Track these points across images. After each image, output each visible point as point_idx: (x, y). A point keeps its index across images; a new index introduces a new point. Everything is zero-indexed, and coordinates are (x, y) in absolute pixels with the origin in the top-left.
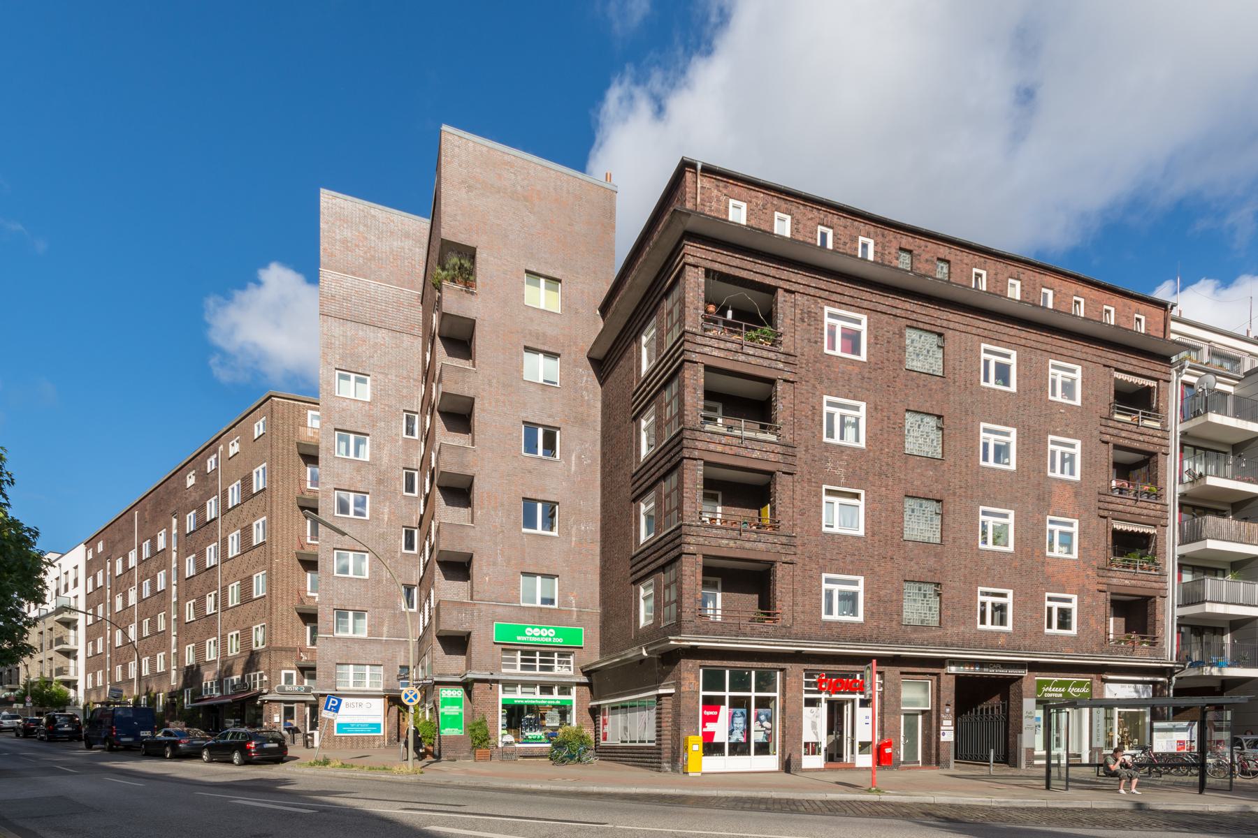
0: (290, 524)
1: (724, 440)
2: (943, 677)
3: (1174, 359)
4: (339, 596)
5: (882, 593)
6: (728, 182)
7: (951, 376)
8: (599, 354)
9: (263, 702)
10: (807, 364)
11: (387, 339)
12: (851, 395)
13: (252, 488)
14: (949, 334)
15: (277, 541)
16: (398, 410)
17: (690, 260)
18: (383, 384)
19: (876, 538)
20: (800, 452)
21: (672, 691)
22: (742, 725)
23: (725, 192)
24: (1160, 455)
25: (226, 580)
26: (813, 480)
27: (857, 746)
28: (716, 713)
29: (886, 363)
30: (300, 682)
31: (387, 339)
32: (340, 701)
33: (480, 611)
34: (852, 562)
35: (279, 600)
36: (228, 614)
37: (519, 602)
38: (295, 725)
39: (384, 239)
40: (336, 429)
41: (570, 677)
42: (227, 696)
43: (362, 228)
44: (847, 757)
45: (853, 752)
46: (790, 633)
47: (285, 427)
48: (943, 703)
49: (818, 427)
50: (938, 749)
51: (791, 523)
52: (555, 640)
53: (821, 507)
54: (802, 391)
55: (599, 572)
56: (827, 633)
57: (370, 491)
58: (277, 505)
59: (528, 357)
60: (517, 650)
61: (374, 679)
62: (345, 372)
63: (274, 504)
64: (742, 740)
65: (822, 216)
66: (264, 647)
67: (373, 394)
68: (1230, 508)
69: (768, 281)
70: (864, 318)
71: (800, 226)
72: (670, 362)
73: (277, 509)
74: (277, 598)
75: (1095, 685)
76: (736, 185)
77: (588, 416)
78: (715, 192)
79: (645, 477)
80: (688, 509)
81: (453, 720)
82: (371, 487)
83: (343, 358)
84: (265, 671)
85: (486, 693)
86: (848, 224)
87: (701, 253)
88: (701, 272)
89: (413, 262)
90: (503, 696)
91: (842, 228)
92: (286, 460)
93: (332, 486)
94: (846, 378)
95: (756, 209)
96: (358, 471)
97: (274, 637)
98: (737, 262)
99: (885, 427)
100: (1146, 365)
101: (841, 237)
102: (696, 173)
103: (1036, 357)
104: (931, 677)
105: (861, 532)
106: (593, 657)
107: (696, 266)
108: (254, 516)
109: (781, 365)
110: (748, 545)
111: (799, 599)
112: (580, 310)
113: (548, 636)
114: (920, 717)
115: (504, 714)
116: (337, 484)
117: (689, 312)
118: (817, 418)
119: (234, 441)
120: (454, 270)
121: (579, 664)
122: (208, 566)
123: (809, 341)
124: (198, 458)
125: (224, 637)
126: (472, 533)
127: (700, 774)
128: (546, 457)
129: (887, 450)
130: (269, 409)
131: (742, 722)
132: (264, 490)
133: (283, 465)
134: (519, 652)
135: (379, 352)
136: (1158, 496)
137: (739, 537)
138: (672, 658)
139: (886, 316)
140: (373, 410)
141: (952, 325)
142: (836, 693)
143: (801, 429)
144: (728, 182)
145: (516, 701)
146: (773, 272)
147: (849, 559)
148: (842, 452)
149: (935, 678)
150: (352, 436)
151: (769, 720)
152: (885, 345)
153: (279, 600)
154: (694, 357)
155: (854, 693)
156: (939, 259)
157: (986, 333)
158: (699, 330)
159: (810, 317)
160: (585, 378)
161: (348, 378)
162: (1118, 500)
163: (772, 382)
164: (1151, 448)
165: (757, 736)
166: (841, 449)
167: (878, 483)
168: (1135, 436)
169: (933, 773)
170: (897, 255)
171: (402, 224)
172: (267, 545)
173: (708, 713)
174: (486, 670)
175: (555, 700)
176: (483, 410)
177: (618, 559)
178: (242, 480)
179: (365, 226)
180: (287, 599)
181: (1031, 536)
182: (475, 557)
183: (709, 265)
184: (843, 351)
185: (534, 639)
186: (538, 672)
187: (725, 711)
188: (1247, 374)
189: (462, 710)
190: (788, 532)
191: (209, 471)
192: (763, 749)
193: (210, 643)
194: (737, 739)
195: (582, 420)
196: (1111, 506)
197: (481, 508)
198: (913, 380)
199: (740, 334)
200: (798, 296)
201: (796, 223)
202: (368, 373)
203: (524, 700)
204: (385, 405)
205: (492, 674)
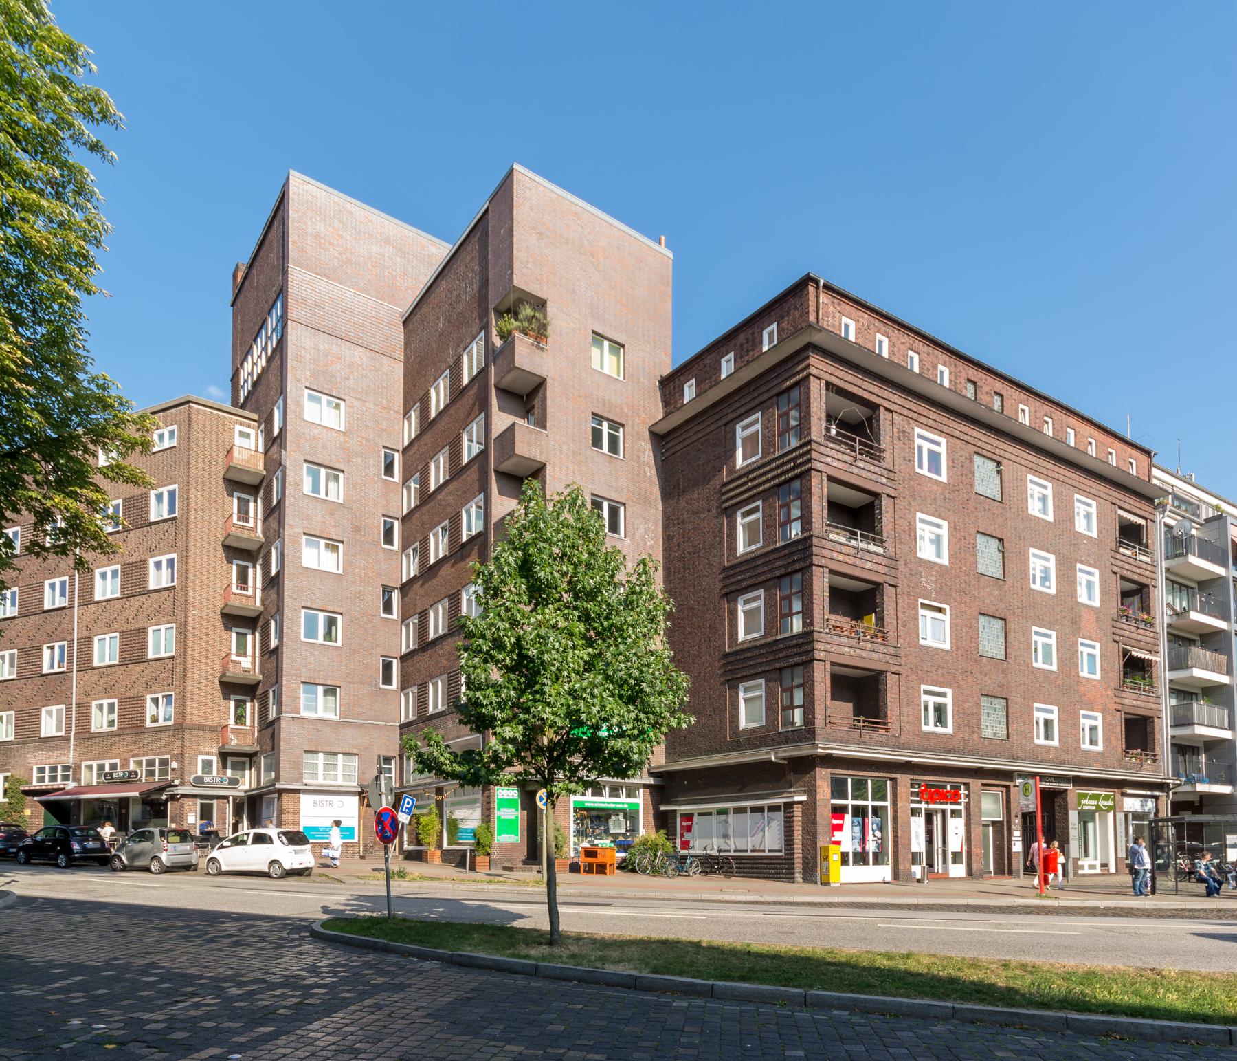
1: (844, 549)
2: (1012, 789)
3: (1156, 501)
5: (966, 705)
7: (1007, 502)
9: (173, 797)
10: (903, 481)
11: (364, 359)
12: (937, 514)
14: (1005, 462)
15: (194, 587)
16: (376, 445)
18: (360, 412)
19: (960, 652)
20: (901, 564)
21: (804, 798)
24: (1151, 587)
27: (950, 857)
28: (840, 822)
29: (961, 486)
31: (364, 359)
35: (196, 663)
36: (91, 677)
39: (362, 242)
43: (336, 224)
44: (939, 867)
45: (945, 861)
48: (1013, 814)
50: (1010, 859)
53: (917, 619)
57: (345, 540)
58: (196, 540)
61: (346, 772)
62: (317, 391)
63: (192, 539)
64: (859, 849)
67: (349, 423)
68: (1198, 638)
69: (873, 398)
71: (896, 349)
72: (788, 466)
73: (195, 546)
75: (1117, 798)
78: (831, 309)
81: (508, 826)
82: (345, 535)
88: (823, 383)
89: (394, 273)
93: (301, 531)
96: (332, 514)
98: (849, 378)
100: (1138, 504)
103: (1066, 490)
104: (1000, 789)
105: (947, 646)
107: (818, 378)
109: (884, 480)
110: (864, 654)
111: (904, 709)
112: (642, 379)
114: (991, 828)
118: (912, 534)
133: (203, 491)
136: (1152, 625)
138: (804, 766)
140: (348, 442)
141: (1007, 455)
143: (901, 543)
146: (876, 390)
147: (940, 671)
149: (1004, 789)
150: (323, 471)
153: (196, 663)
155: (947, 803)
156: (996, 393)
157: (1030, 465)
161: (318, 401)
162: (1126, 627)
163: (877, 495)
164: (1144, 581)
165: (872, 847)
168: (1134, 569)
169: (1007, 882)
173: (835, 822)
179: (340, 222)
180: (206, 663)
181: (1069, 657)
187: (848, 818)
188: (1208, 520)
192: (878, 859)
196: (1122, 632)
198: (981, 503)
201: (892, 345)
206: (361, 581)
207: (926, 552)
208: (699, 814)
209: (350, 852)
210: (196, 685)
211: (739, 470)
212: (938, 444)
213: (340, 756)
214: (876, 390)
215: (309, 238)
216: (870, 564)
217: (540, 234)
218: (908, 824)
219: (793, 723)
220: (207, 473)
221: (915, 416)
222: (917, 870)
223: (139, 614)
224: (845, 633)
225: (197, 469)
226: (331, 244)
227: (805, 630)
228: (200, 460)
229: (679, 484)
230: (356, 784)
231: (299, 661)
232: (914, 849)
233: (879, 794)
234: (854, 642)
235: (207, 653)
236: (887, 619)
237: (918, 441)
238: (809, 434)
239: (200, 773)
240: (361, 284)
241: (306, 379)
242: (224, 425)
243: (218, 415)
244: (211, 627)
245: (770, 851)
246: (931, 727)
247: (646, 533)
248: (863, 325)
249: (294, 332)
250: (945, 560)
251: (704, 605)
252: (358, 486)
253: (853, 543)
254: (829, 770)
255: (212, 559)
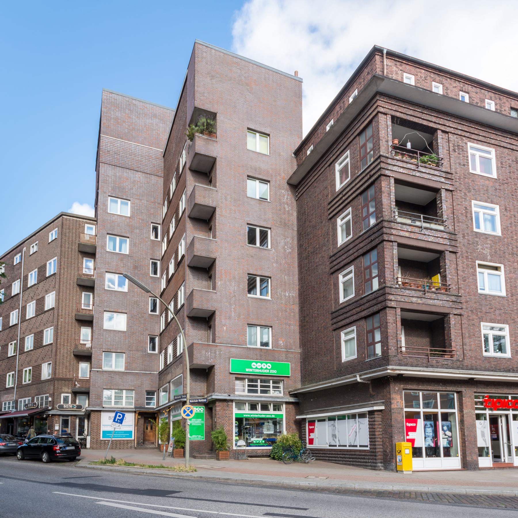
0: (71, 296)
4: (107, 343)
6: (402, 62)
8: (295, 181)
10: (460, 179)
11: (141, 178)
12: (489, 200)
13: (46, 273)
15: (62, 307)
17: (381, 110)
19: (514, 297)
20: (460, 238)
21: (383, 408)
22: (431, 434)
23: (401, 68)
25: (24, 333)
26: (470, 257)
28: (414, 425)
29: (510, 180)
30: (74, 401)
31: (141, 178)
32: (124, 415)
33: (221, 351)
34: (500, 315)
37: (246, 344)
38: (69, 432)
39: (141, 119)
40: (108, 234)
41: (282, 398)
42: (21, 412)
43: (127, 111)
44: (505, 458)
46: (462, 365)
47: (71, 234)
49: (470, 221)
51: (457, 287)
52: (272, 371)
53: (476, 275)
54: (458, 197)
55: (298, 324)
56: (488, 365)
58: (63, 283)
59: (250, 183)
60: (244, 379)
63: (62, 283)
64: (432, 445)
65: (462, 86)
66: (30, 382)
67: (132, 212)
69: (431, 125)
70: (493, 150)
73: (63, 287)
74: (60, 345)
76: (408, 64)
77: (289, 221)
78: (395, 68)
79: (343, 257)
80: (389, 276)
83: (114, 189)
84: (50, 394)
85: (224, 410)
86: (478, 91)
87: (388, 106)
88: (389, 118)
89: (159, 132)
90: (236, 412)
91: (475, 94)
92: (70, 255)
93: (105, 270)
94: (486, 189)
95: (421, 80)
96: (122, 260)
97: (57, 371)
98: (411, 112)
99: (513, 222)
101: (475, 99)
102: (382, 56)
105: (504, 294)
106: (298, 386)
107: (385, 114)
108: (46, 291)
109: (443, 180)
111: (467, 341)
112: (282, 154)
113: (266, 369)
115: (237, 425)
116: (108, 269)
117: (383, 143)
118: (469, 215)
119: (34, 244)
120: (204, 126)
121: (287, 388)
122: (11, 325)
123: (460, 164)
124: (8, 256)
125: (20, 372)
126: (214, 296)
127: (411, 472)
128: (261, 247)
129: (515, 237)
130: (60, 223)
131: (431, 431)
132: (54, 274)
133: (68, 258)
134: (246, 380)
135: (136, 186)
137: (424, 296)
139: (507, 150)
140: (131, 222)
142: (495, 410)
143: (459, 222)
144: (402, 62)
145: (244, 416)
146: (434, 119)
147: (497, 312)
148: (487, 238)
150: (118, 238)
151: (450, 430)
152: (508, 168)
154: (387, 173)
155: (509, 410)
158: (389, 155)
159: (459, 149)
160: (286, 197)
161: (116, 202)
163: (437, 191)
165: (443, 443)
166: (486, 236)
167: (512, 259)
170: (509, 111)
171: (152, 109)
172: (55, 310)
173: (409, 425)
174: (225, 393)
175: (271, 415)
176: (221, 216)
177: (318, 314)
178: (38, 269)
179: (129, 110)
180: (67, 346)
182: (217, 313)
183: (394, 113)
184: (481, 171)
185: (257, 371)
186: (259, 394)
187: (421, 422)
189: (204, 422)
190: (455, 293)
191: (15, 264)
192: (447, 453)
193: (10, 375)
194: (429, 445)
195: (285, 223)
197: (221, 280)
199: (416, 158)
200: (450, 135)
201: (445, 88)
202: (129, 199)
203: (250, 414)
204: (140, 219)
205: (229, 396)
206: (138, 295)
207: (484, 228)
208: (319, 421)
209: (129, 445)
210: (62, 357)
211: (338, 192)
212: (489, 153)
213: (124, 391)
214: (434, 119)
215: (112, 120)
216: (433, 238)
217: (213, 76)
218: (474, 426)
219: (375, 354)
220: (70, 249)
221: (467, 135)
222: (486, 462)
223: (41, 324)
224: (412, 288)
225: (65, 248)
226: (125, 122)
227: (381, 287)
228: (67, 243)
229: (305, 212)
230: (133, 406)
231: (102, 340)
232: (481, 443)
233: (448, 403)
234: (420, 294)
235: (68, 341)
236: (449, 277)
237: (470, 151)
238: (379, 152)
239: (62, 403)
240: (140, 140)
241: (109, 192)
242: (80, 225)
243: (76, 220)
244: (70, 327)
245: (360, 446)
246: (492, 353)
247: (285, 245)
248: (421, 77)
249: (103, 168)
250: (498, 232)
251: (320, 283)
252: (137, 245)
253: (418, 223)
254: (402, 386)
255: (71, 292)
